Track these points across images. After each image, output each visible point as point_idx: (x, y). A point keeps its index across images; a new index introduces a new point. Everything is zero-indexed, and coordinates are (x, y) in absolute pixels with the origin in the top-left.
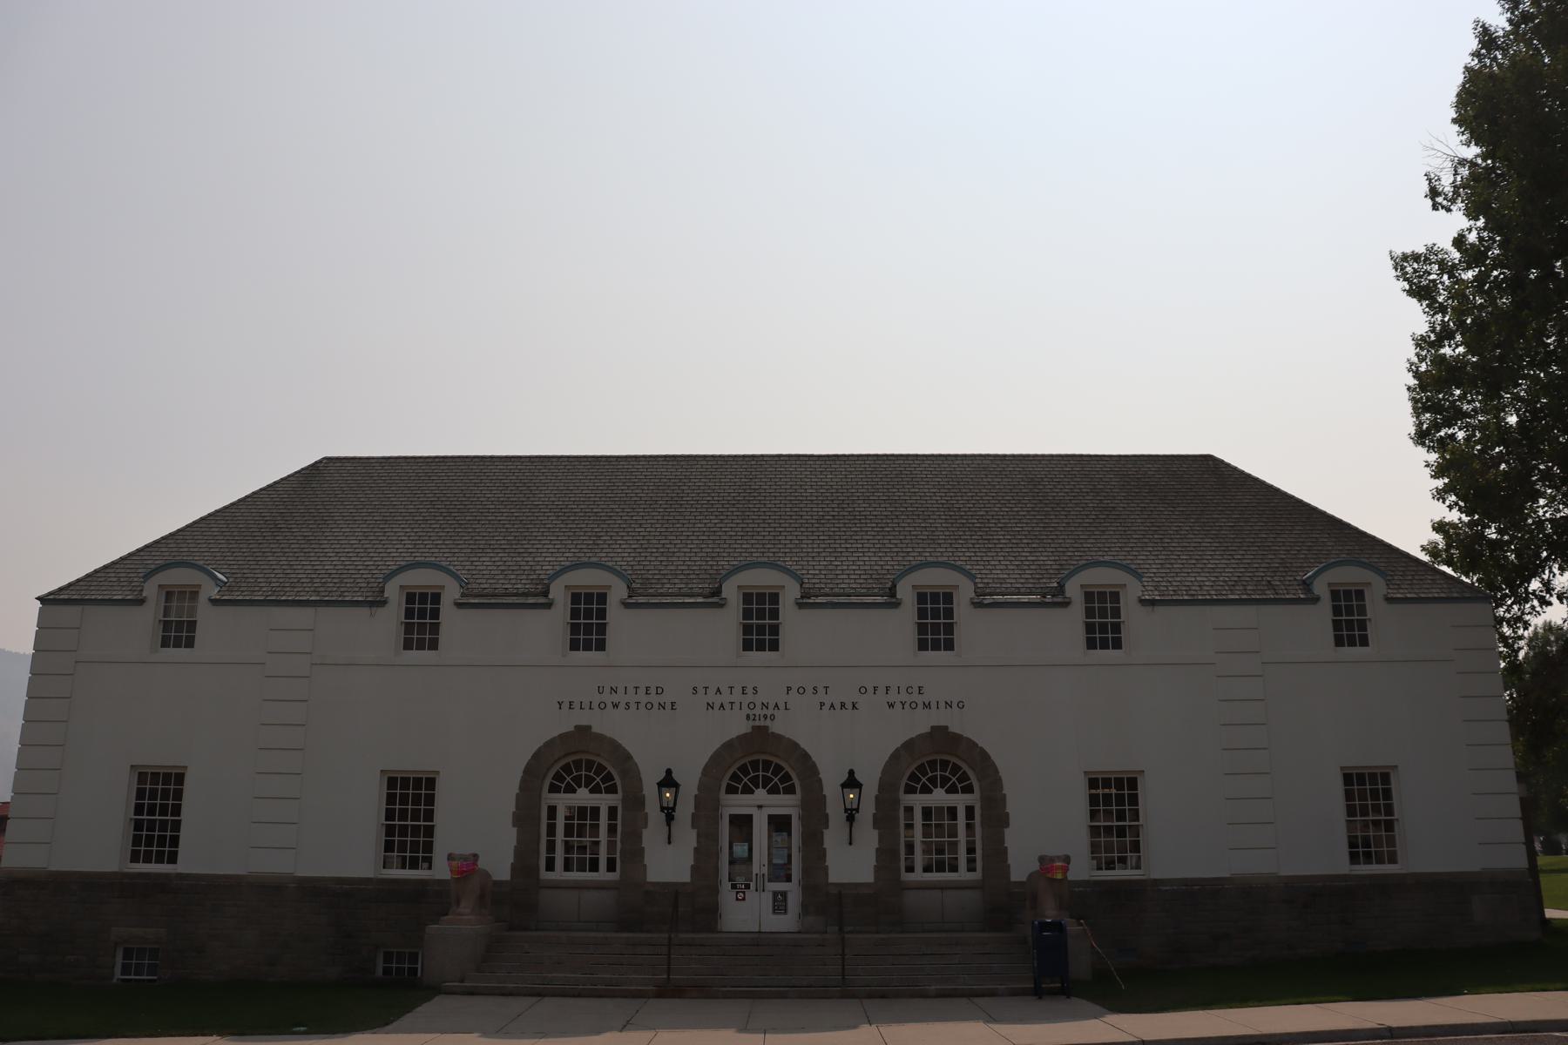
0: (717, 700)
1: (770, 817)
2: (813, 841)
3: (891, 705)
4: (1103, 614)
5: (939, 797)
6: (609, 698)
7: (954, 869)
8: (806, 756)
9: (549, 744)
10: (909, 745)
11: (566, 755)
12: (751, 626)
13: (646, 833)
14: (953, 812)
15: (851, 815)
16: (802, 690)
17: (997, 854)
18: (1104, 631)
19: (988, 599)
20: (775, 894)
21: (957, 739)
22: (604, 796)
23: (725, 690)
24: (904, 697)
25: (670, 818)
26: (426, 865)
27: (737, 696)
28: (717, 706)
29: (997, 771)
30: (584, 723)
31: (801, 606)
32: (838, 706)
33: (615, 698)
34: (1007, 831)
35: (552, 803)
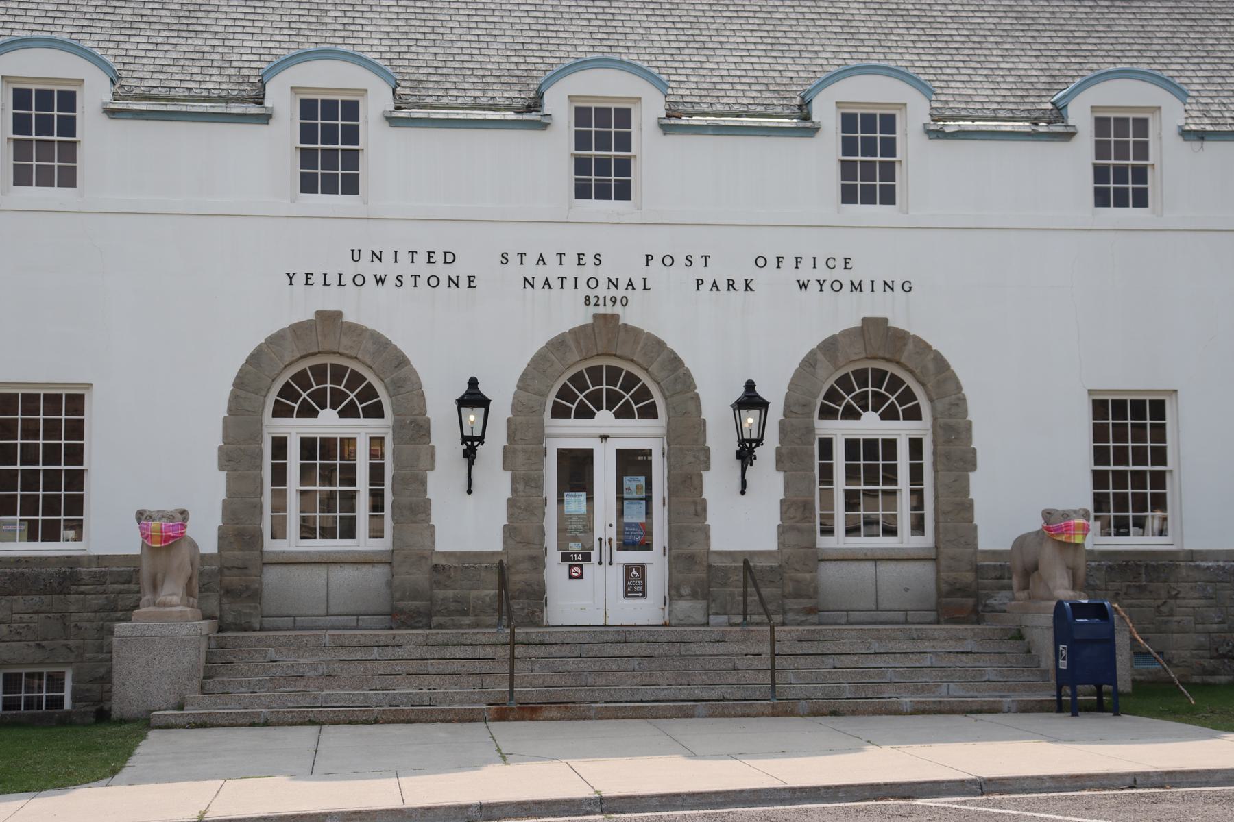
0: (540, 274)
1: (619, 453)
2: (687, 485)
3: (803, 286)
4: (1122, 152)
5: (870, 425)
6: (369, 268)
7: (891, 531)
8: (675, 361)
9: (275, 340)
10: (830, 347)
11: (303, 357)
12: (1107, 167)
13: (432, 478)
14: (349, 442)
15: (471, 446)
16: (668, 261)
17: (958, 510)
18: (1121, 179)
19: (952, 126)
20: (628, 568)
21: (900, 338)
22: (362, 421)
23: (552, 259)
24: (822, 273)
25: (470, 454)
26: (71, 534)
27: (570, 268)
28: (539, 283)
29: (959, 387)
30: (331, 307)
31: (666, 129)
32: (723, 285)
34: (973, 476)
35: (280, 432)
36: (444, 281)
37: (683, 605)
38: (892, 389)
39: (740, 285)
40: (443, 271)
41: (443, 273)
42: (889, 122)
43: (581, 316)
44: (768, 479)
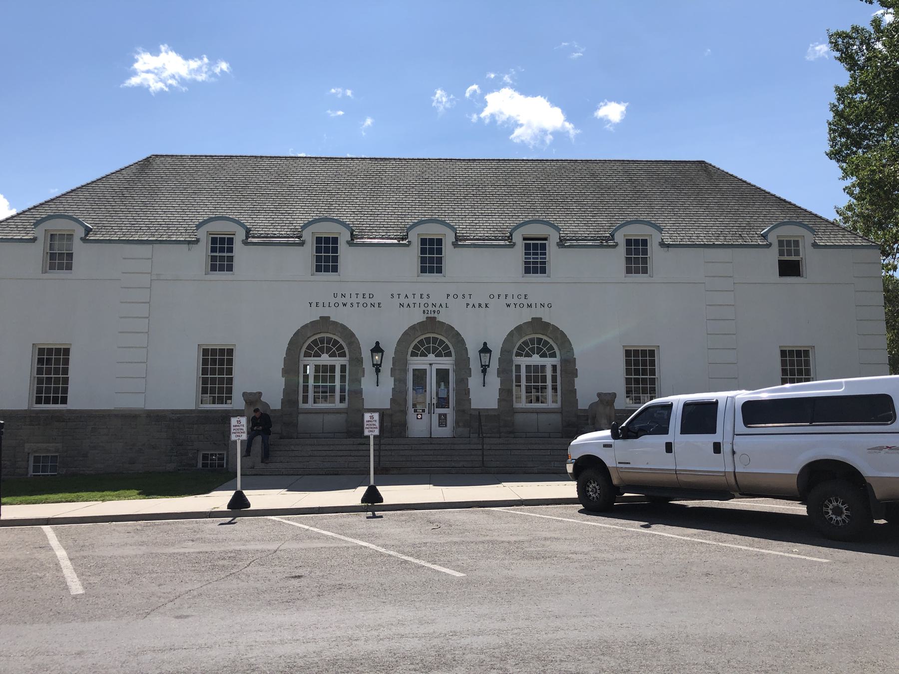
0: (406, 301)
2: (462, 382)
14: (543, 367)
15: (484, 369)
16: (456, 296)
17: (570, 393)
20: (440, 415)
24: (516, 300)
25: (484, 371)
27: (417, 300)
28: (406, 305)
33: (344, 300)
36: (369, 305)
37: (460, 429)
38: (544, 346)
39: (483, 305)
40: (369, 301)
41: (370, 302)
42: (645, 242)
43: (421, 318)
44: (494, 380)
